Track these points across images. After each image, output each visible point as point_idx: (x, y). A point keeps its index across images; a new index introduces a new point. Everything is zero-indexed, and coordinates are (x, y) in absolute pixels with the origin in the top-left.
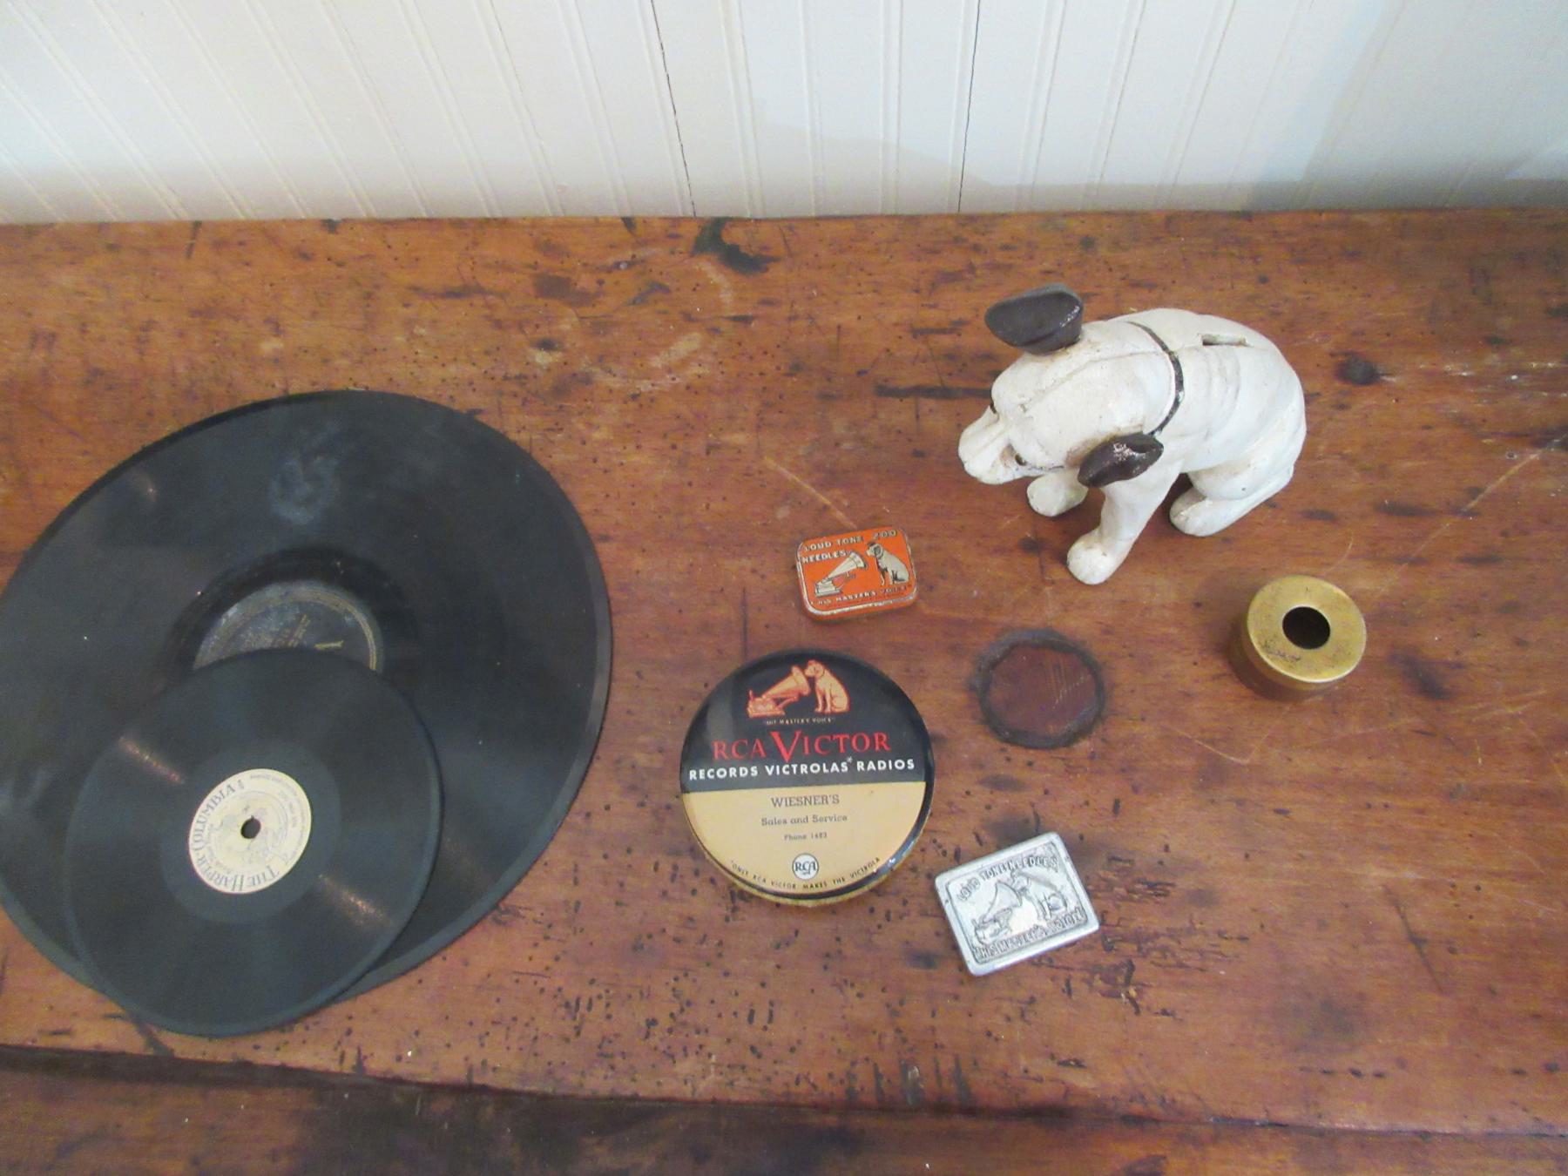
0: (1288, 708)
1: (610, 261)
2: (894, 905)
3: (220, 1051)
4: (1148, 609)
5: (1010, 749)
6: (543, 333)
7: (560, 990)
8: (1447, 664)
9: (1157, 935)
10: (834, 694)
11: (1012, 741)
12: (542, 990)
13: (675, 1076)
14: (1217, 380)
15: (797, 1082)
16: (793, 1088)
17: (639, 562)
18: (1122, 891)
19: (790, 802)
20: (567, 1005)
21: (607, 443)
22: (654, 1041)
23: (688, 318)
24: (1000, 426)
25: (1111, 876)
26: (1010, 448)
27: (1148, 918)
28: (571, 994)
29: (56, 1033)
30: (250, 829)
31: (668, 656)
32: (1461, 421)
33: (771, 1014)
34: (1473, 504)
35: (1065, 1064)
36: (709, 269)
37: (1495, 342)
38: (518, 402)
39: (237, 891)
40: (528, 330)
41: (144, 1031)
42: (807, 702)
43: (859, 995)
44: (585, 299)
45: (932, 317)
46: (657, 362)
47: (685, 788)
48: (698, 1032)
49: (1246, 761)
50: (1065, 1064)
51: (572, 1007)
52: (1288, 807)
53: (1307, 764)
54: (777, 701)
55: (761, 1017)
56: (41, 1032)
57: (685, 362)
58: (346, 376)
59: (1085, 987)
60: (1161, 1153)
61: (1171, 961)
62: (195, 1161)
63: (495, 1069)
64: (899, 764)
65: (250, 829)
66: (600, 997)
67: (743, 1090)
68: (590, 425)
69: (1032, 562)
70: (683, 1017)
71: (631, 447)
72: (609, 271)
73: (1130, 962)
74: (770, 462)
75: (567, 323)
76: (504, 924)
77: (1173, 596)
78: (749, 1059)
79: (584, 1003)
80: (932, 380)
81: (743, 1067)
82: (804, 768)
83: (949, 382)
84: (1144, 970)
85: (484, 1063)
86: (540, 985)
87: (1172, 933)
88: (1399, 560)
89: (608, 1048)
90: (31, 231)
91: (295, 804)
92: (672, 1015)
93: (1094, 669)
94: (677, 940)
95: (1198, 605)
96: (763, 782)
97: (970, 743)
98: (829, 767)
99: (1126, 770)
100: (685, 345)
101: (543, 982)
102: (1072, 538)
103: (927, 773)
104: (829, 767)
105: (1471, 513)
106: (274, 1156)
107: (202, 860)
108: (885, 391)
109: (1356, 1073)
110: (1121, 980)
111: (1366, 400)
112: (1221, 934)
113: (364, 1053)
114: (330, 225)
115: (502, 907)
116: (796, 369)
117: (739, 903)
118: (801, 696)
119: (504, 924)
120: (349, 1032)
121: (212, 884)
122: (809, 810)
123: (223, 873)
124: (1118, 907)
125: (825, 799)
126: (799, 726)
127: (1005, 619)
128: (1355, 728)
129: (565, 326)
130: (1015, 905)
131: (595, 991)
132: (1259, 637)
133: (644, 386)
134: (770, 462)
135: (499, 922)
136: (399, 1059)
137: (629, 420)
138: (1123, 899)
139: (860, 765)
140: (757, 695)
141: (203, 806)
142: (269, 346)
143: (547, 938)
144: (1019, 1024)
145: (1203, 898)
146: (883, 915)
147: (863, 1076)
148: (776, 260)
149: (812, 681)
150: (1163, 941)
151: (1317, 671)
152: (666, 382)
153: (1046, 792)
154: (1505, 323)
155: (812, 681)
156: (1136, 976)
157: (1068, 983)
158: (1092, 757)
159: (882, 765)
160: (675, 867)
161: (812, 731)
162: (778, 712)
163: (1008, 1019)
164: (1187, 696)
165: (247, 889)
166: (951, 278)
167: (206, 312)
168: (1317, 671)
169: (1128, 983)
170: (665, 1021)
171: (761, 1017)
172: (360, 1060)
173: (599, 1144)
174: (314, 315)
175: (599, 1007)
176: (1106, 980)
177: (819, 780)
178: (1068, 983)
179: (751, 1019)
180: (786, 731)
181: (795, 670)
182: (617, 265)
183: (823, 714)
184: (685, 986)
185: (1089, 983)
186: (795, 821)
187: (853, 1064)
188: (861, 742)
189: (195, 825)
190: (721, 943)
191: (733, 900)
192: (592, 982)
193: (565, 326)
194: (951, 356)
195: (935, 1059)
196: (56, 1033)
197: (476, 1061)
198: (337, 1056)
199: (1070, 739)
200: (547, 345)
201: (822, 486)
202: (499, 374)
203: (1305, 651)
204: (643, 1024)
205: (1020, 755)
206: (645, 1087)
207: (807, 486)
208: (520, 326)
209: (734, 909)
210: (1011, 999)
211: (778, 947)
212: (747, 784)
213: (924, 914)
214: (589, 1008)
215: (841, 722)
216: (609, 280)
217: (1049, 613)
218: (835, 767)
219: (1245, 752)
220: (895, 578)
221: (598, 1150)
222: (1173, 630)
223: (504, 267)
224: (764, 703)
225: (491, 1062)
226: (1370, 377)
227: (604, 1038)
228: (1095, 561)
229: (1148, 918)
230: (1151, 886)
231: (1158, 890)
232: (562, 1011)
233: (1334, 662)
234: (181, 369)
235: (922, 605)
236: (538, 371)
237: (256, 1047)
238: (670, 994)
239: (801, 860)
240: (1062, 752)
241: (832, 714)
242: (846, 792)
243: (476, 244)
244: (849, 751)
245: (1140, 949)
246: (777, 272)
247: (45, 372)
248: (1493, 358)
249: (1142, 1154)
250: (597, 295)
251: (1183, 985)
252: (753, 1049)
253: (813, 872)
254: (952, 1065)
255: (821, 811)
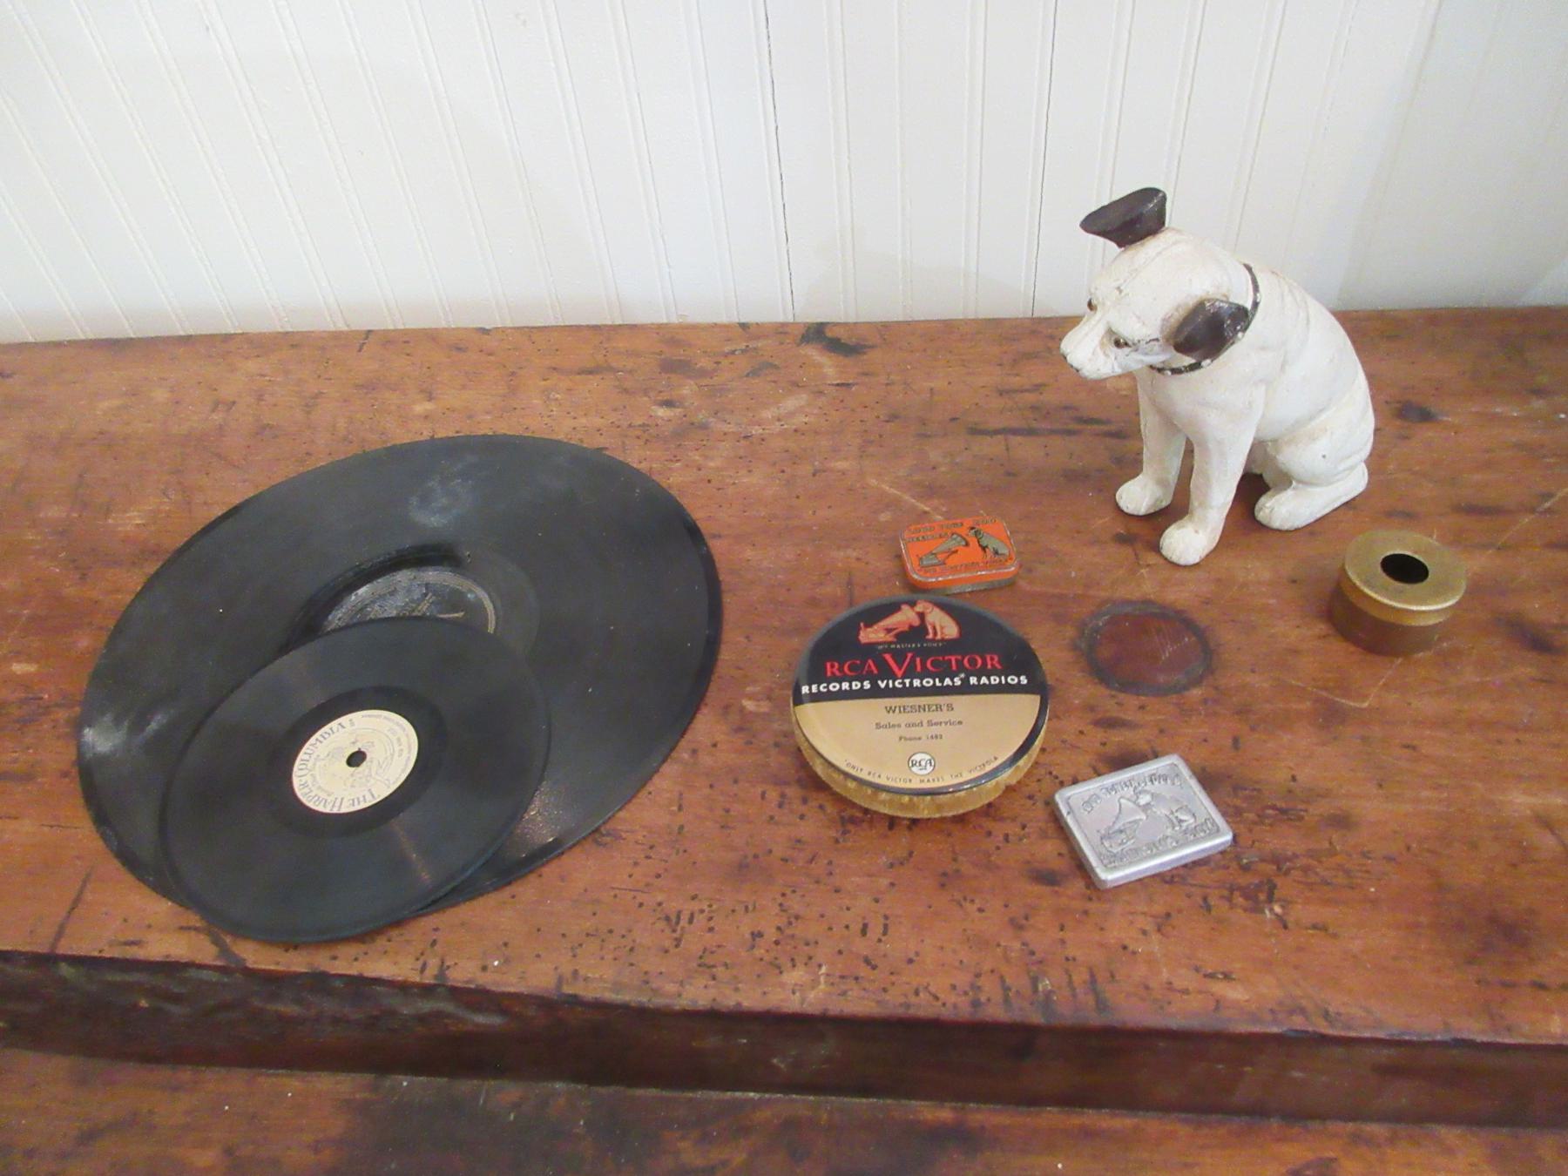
0: (1400, 660)
1: (727, 349)
2: (1013, 829)
3: (296, 962)
4: (1245, 585)
5: (1122, 696)
6: (665, 396)
7: (660, 904)
8: (1556, 627)
9: (1295, 856)
10: (945, 627)
11: (1124, 688)
12: (641, 905)
13: (782, 985)
14: (1289, 299)
15: (917, 993)
16: (913, 999)
17: (749, 553)
18: (1251, 816)
19: (904, 709)
20: (668, 919)
21: (718, 469)
22: (759, 952)
23: (796, 384)
24: (1099, 314)
25: (1238, 802)
26: (1110, 332)
27: (1288, 841)
28: (672, 906)
29: (133, 943)
30: (356, 759)
31: (777, 624)
32: (1519, 446)
33: (886, 927)
34: (1547, 505)
35: (1211, 976)
36: (813, 353)
37: (1539, 392)
38: (641, 442)
39: (335, 811)
40: (652, 394)
41: (216, 942)
42: (918, 631)
43: (980, 910)
44: (703, 373)
45: (1015, 381)
46: (767, 414)
47: (799, 700)
48: (807, 944)
49: (1365, 705)
50: (1211, 976)
51: (672, 921)
52: (1415, 743)
53: (1426, 705)
54: (889, 631)
55: (875, 931)
56: (111, 944)
57: (791, 414)
58: (486, 425)
59: (1226, 905)
60: (1332, 1154)
61: (1312, 878)
62: (228, 1151)
63: (586, 979)
64: (1012, 680)
65: (356, 759)
66: (702, 911)
67: (858, 1003)
68: (706, 457)
69: (1126, 551)
70: (789, 932)
71: (744, 472)
72: (726, 355)
73: (1270, 881)
74: (873, 482)
75: (687, 389)
76: (605, 845)
77: (1266, 575)
78: (864, 971)
79: (685, 918)
80: (1015, 424)
81: (856, 979)
82: (916, 683)
83: (1035, 425)
84: (1285, 887)
85: (575, 972)
86: (639, 900)
87: (1311, 854)
88: (1486, 547)
89: (708, 960)
90: (227, 338)
91: (404, 740)
92: (779, 928)
93: (1201, 635)
94: (785, 860)
95: (1294, 582)
96: (875, 693)
97: (1081, 689)
98: (942, 681)
99: (1243, 712)
100: (791, 403)
101: (641, 897)
102: (1160, 531)
103: (1038, 686)
104: (942, 681)
105: (1549, 511)
106: (315, 1148)
107: (305, 785)
108: (975, 431)
109: (1542, 987)
110: (1262, 897)
111: (1428, 433)
112: (1365, 855)
113: (447, 963)
114: (484, 331)
115: (603, 830)
116: (893, 417)
117: (851, 827)
118: (911, 627)
119: (605, 845)
120: (434, 943)
121: (311, 805)
122: (925, 717)
123: (323, 795)
124: (1250, 831)
125: (939, 708)
126: (910, 650)
127: (1103, 594)
128: (1470, 676)
129: (686, 391)
130: (1144, 818)
131: (695, 906)
132: (1359, 575)
133: (756, 431)
134: (873, 482)
135: (596, 841)
136: (484, 968)
137: (742, 453)
138: (1255, 823)
139: (973, 680)
140: (867, 626)
141: (312, 740)
142: (421, 408)
143: (648, 857)
144: (1155, 937)
145: (1341, 821)
146: (1001, 838)
147: (990, 989)
148: (872, 347)
149: (922, 616)
150: (1303, 861)
151: (1425, 607)
152: (777, 427)
153: (1162, 731)
154: (1543, 380)
155: (922, 616)
156: (1277, 893)
157: (1205, 899)
158: (1205, 701)
159: (995, 680)
160: (783, 795)
161: (924, 653)
162: (889, 638)
163: (1144, 932)
164: (1295, 652)
165: (346, 809)
166: (1029, 356)
167: (369, 387)
168: (1425, 607)
169: (1270, 899)
170: (771, 934)
171: (875, 931)
172: (443, 968)
173: (683, 1138)
174: (464, 387)
175: (700, 919)
176: (1247, 897)
177: (934, 691)
178: (1205, 899)
179: (864, 931)
180: (899, 656)
181: (905, 608)
182: (733, 352)
183: (933, 640)
184: (795, 904)
185: (1229, 900)
186: (908, 725)
187: (978, 975)
188: (973, 662)
189: (301, 755)
190: (830, 863)
191: (843, 824)
192: (694, 898)
193: (686, 391)
194: (1033, 408)
195: (1067, 971)
196: (133, 943)
197: (566, 969)
198: (420, 963)
199: (1180, 689)
200: (668, 404)
201: (920, 497)
202: (626, 424)
203: (1407, 587)
204: (748, 936)
205: (1132, 701)
206: (750, 998)
207: (906, 497)
208: (646, 392)
209: (844, 833)
210: (1144, 914)
211: (892, 865)
212: (861, 694)
213: (1044, 835)
214: (691, 921)
215: (949, 646)
216: (725, 362)
217: (1147, 586)
218: (947, 681)
219: (1365, 697)
220: (996, 553)
221: (682, 1145)
222: (1272, 601)
223: (636, 354)
224: (876, 632)
225: (582, 972)
226: (1426, 416)
227: (705, 950)
228: (1189, 542)
229: (1288, 841)
230: (1283, 811)
231: (1286, 815)
232: (661, 925)
233: (1438, 594)
234: (342, 424)
235: (1022, 583)
236: (660, 422)
237: (335, 958)
238: (777, 910)
239: (917, 757)
240: (1174, 698)
241: (943, 640)
242: (960, 701)
243: (609, 339)
244: (961, 668)
245: (1279, 869)
246: (874, 356)
247: (221, 427)
248: (1538, 404)
249: (1310, 1156)
250: (715, 370)
251: (1327, 902)
252: (867, 961)
253: (929, 769)
254: (1087, 977)
255: (936, 716)
